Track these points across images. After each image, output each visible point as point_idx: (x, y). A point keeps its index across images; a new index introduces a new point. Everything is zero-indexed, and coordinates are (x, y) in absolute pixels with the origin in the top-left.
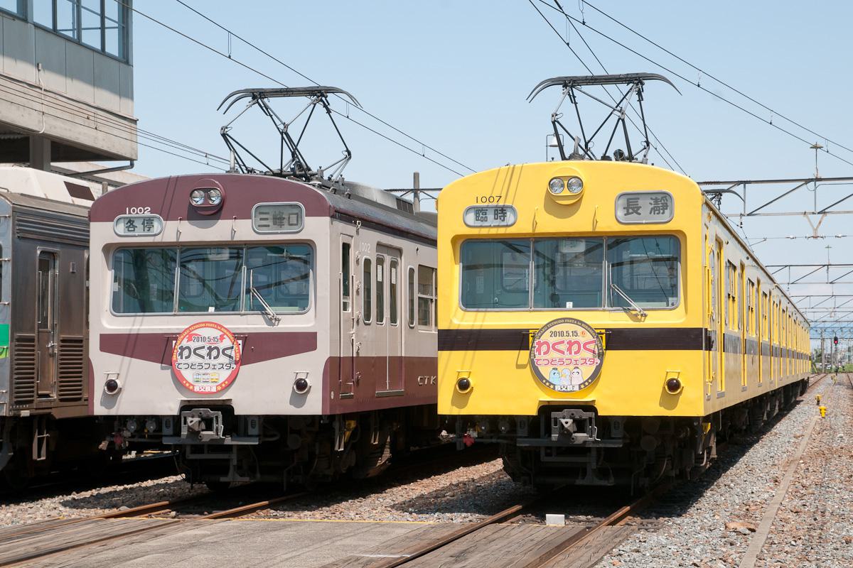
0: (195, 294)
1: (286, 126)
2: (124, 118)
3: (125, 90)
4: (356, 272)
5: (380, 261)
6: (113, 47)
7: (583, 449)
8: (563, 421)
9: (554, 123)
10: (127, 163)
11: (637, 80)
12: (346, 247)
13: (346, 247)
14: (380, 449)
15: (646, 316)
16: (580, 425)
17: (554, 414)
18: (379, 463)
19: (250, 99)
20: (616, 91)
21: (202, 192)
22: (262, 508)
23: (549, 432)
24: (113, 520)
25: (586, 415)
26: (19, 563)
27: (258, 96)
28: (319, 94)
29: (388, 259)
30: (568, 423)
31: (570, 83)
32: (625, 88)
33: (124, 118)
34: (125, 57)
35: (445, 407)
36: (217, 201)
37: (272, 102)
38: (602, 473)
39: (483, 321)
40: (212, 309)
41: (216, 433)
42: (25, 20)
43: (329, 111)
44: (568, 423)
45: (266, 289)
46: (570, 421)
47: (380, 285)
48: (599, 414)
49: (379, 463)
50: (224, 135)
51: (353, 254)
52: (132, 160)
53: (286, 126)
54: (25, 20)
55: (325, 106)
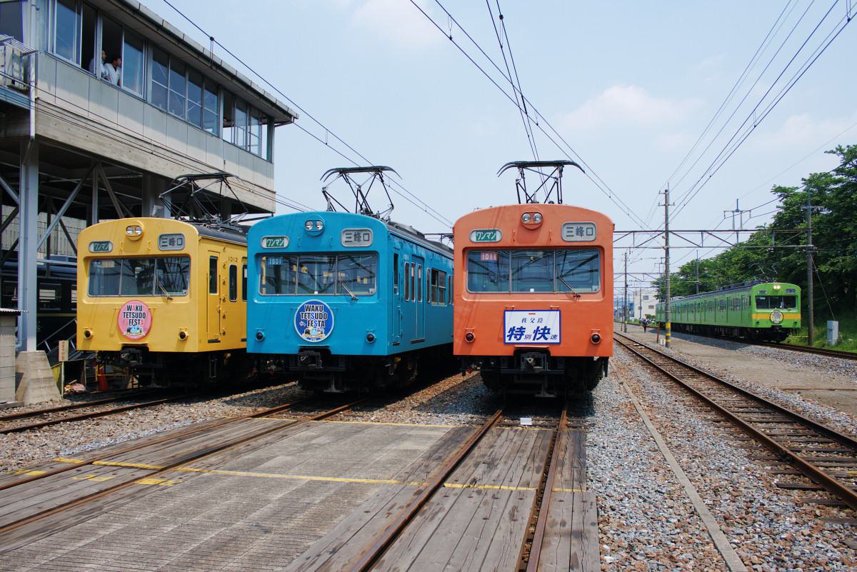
0: (41, 294)
1: (360, 187)
2: (269, 191)
3: (270, 174)
4: (401, 269)
5: (413, 266)
6: (264, 156)
7: (541, 375)
8: (528, 359)
9: (517, 184)
10: (270, 215)
11: (559, 165)
12: (396, 256)
13: (396, 256)
14: (413, 371)
15: (579, 296)
16: (538, 362)
17: (523, 355)
18: (411, 378)
19: (338, 173)
20: (548, 170)
21: (311, 222)
22: (342, 410)
23: (519, 365)
24: (256, 419)
25: (542, 356)
26: (191, 462)
27: (343, 172)
28: (378, 170)
29: (417, 265)
30: (531, 360)
31: (522, 165)
32: (553, 168)
33: (269, 191)
34: (270, 159)
35: (457, 351)
36: (320, 228)
37: (351, 175)
38: (549, 390)
39: (124, 274)
40: (316, 293)
41: (318, 366)
42: (218, 137)
43: (382, 181)
44: (531, 360)
45: (589, 273)
46: (532, 360)
47: (413, 278)
48: (552, 355)
49: (411, 378)
50: (324, 192)
51: (399, 259)
52: (272, 213)
53: (360, 187)
54: (218, 137)
55: (381, 178)
